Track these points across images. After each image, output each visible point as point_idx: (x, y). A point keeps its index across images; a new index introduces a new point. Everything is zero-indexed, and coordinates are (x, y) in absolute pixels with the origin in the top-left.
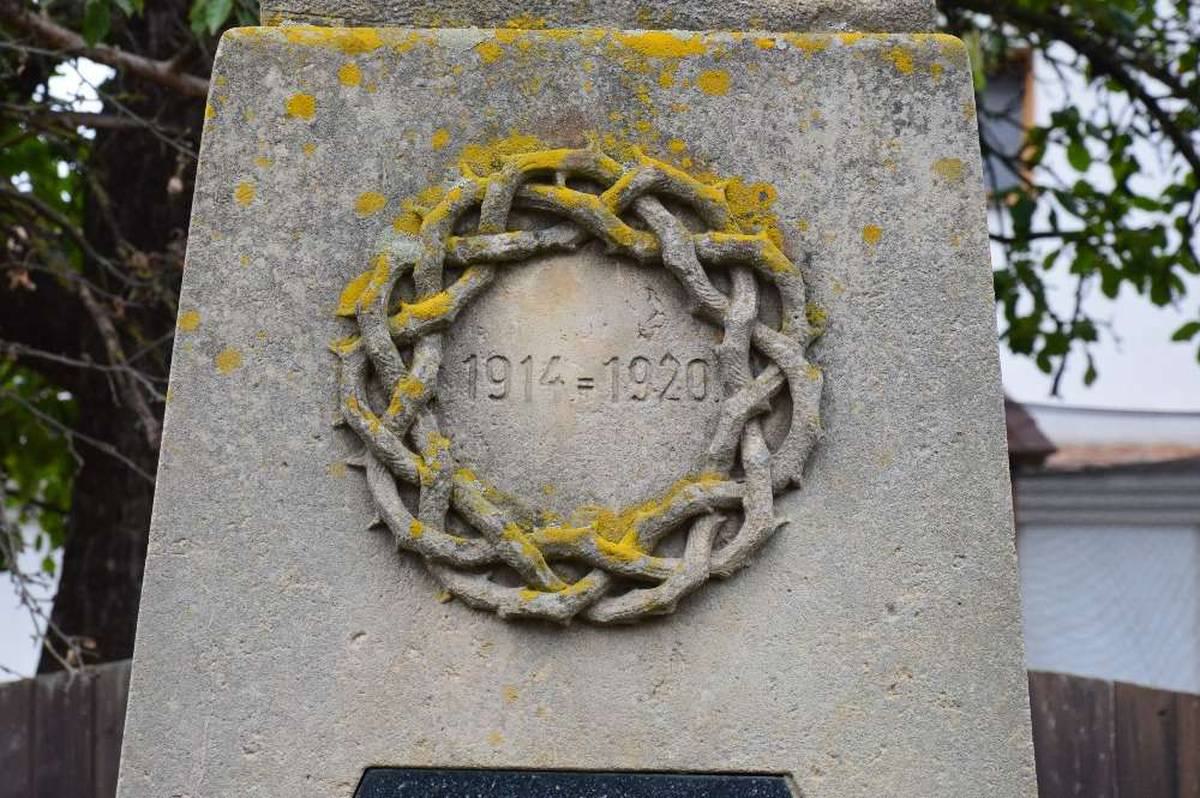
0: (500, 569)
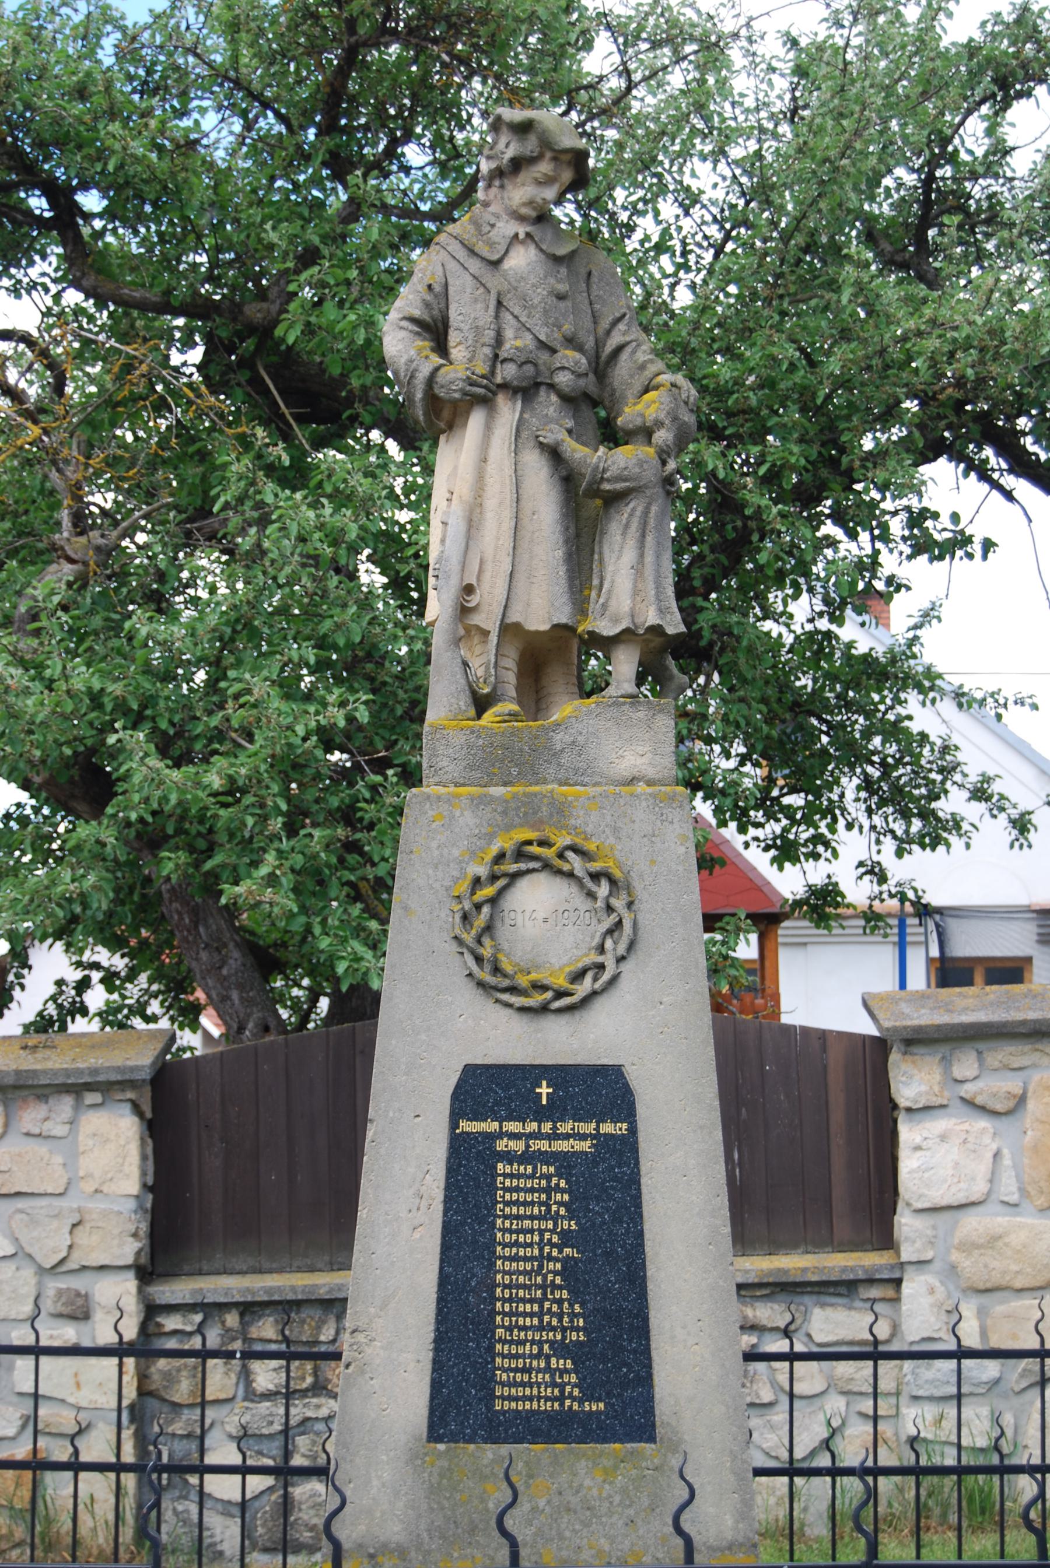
0: (513, 990)
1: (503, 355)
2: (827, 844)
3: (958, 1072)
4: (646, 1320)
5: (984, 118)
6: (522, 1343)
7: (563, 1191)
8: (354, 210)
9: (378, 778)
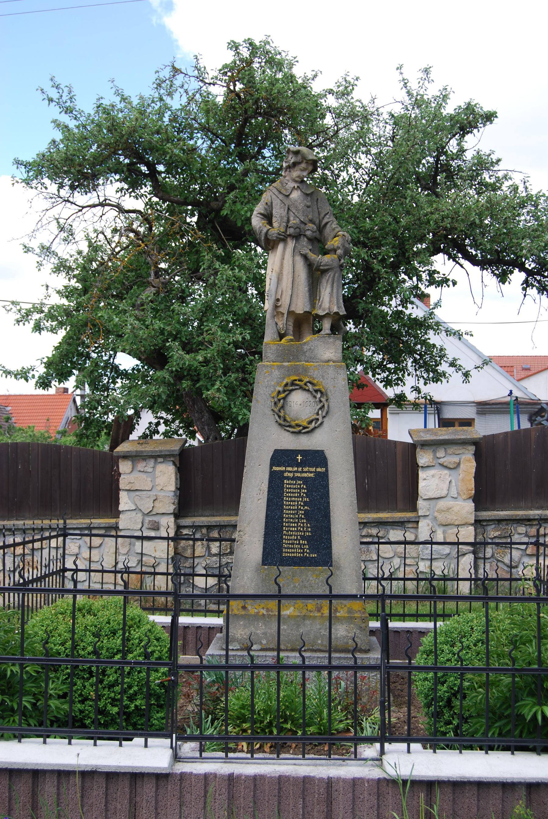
0: (290, 426)
1: (289, 225)
2: (402, 381)
3: (438, 455)
4: (330, 529)
5: (456, 139)
6: (291, 535)
7: (305, 489)
8: (245, 173)
9: (252, 358)
